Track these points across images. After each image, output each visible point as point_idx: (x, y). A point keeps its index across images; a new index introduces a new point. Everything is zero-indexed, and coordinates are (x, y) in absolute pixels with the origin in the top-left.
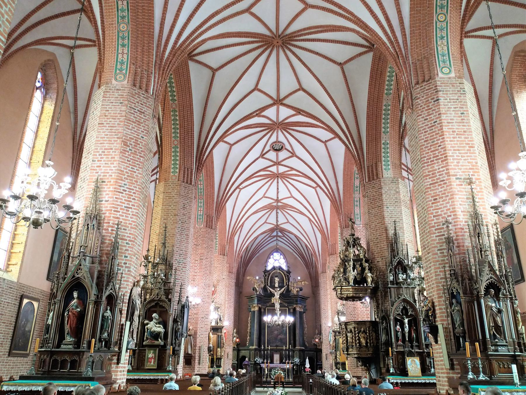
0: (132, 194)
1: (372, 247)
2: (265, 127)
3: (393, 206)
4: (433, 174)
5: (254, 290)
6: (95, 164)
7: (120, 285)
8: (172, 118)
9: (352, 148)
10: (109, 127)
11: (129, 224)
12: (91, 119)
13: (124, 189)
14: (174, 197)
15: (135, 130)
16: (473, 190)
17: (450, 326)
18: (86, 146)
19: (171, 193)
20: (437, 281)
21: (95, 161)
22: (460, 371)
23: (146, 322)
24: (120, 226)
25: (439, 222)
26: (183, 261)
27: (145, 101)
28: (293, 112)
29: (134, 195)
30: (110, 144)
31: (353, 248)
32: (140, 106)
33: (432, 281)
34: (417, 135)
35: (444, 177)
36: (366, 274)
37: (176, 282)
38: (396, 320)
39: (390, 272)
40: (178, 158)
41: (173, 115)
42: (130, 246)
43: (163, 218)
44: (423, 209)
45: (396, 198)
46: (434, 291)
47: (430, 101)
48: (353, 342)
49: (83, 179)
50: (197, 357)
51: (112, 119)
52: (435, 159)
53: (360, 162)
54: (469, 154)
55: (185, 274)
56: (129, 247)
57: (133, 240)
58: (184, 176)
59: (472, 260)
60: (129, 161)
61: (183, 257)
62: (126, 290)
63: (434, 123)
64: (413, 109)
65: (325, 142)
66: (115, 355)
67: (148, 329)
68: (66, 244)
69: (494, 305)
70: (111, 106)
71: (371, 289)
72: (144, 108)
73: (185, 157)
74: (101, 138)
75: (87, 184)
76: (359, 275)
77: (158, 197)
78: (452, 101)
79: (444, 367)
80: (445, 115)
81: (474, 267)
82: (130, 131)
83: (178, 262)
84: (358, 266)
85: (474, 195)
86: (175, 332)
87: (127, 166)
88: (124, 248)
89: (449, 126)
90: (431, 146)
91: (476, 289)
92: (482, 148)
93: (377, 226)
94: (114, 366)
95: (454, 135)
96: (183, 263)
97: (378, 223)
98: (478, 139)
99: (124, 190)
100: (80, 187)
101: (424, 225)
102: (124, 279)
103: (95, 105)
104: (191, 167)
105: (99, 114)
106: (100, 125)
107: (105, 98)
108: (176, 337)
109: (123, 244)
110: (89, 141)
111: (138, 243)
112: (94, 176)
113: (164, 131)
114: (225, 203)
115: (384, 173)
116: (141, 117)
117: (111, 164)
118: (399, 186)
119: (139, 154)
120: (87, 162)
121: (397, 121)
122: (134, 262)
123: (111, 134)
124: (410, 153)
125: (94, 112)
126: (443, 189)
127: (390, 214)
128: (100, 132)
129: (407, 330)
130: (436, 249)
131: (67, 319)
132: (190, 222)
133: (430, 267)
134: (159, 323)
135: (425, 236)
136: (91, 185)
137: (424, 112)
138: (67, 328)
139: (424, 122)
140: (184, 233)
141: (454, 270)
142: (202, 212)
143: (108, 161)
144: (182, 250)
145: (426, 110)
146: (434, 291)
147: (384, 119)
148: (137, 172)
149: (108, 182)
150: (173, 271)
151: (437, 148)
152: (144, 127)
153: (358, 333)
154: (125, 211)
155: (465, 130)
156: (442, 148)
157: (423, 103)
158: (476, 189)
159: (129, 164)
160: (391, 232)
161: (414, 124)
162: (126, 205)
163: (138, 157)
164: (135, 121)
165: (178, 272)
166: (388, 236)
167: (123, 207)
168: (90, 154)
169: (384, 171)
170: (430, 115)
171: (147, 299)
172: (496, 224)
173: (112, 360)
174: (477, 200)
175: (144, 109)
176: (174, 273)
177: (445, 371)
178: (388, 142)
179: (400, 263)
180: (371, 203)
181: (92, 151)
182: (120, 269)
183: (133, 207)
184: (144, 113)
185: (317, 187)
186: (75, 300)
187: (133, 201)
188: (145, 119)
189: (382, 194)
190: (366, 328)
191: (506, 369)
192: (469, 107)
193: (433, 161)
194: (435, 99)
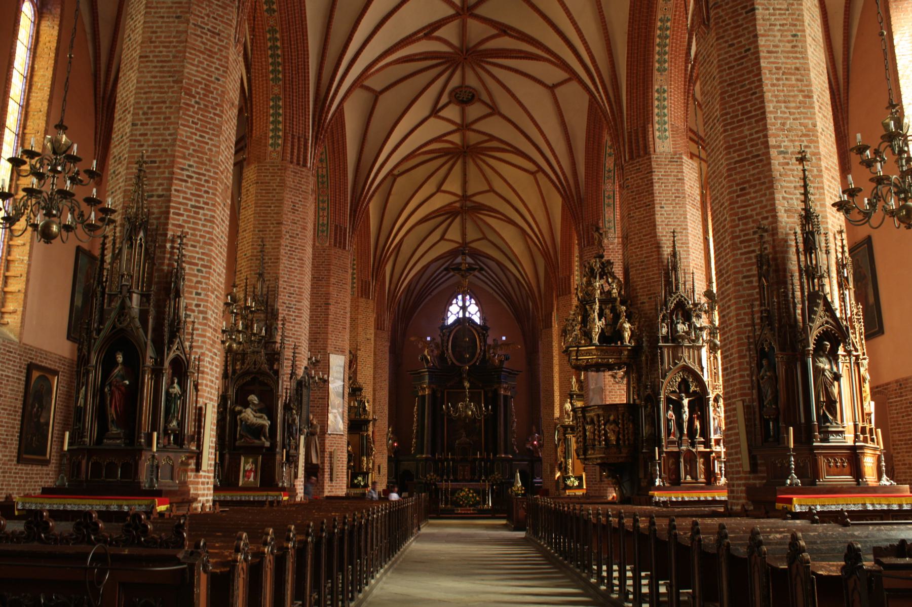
0: (203, 183)
1: (633, 278)
2: (442, 58)
3: (671, 204)
4: (740, 144)
5: (422, 360)
6: (136, 130)
7: (192, 342)
8: (269, 44)
9: (601, 98)
10: (158, 62)
11: (201, 236)
12: (126, 49)
13: (188, 173)
14: (275, 190)
15: (205, 66)
16: (807, 173)
17: (755, 404)
18: (120, 99)
19: (269, 183)
20: (739, 329)
21: (136, 125)
22: (765, 475)
23: (238, 408)
24: (185, 241)
25: (747, 229)
26: (295, 305)
27: (220, 13)
28: (494, 32)
29: (206, 185)
30: (161, 93)
31: (600, 279)
32: (212, 23)
33: (730, 330)
34: (715, 74)
35: (759, 150)
36: (622, 324)
37: (285, 342)
38: (669, 400)
39: (663, 321)
40: (281, 119)
41: (270, 39)
42: (204, 275)
43: (257, 230)
44: (721, 206)
45: (677, 190)
46: (733, 348)
47: (740, 11)
48: (594, 439)
49: (117, 158)
50: (327, 470)
51: (164, 47)
52: (744, 117)
53: (616, 125)
54: (802, 110)
55: (300, 328)
56: (203, 277)
57: (209, 264)
58: (292, 152)
59: (798, 294)
60: (196, 124)
61: (295, 298)
62: (203, 351)
63: (746, 51)
64: (709, 26)
65: (552, 88)
66: (192, 458)
67: (241, 421)
68: (97, 272)
69: (827, 367)
70: (160, 24)
71: (628, 350)
72: (219, 25)
73: (293, 117)
74: (145, 83)
75: (124, 167)
76: (609, 327)
77: (248, 190)
78: (778, 12)
79: (741, 469)
80: (764, 39)
81: (799, 306)
82: (195, 68)
83: (287, 307)
84: (607, 311)
85: (808, 182)
86: (289, 427)
87: (192, 133)
88: (195, 279)
89: (770, 57)
90: (739, 93)
91: (801, 341)
92: (825, 100)
93: (642, 240)
94: (192, 474)
95: (778, 74)
96: (296, 309)
97: (644, 236)
98: (819, 82)
99: (188, 176)
100: (114, 172)
101: (721, 235)
102: (198, 332)
103: (131, 23)
104: (305, 135)
105: (140, 39)
106: (142, 59)
107: (148, 10)
108: (291, 434)
109: (192, 272)
110: (124, 89)
111: (218, 270)
112: (137, 151)
113: (255, 69)
114: (368, 203)
115: (657, 144)
116: (213, 43)
117: (164, 129)
118: (682, 169)
119: (212, 111)
120: (123, 127)
121: (683, 50)
122: (212, 303)
123: (162, 75)
124: (703, 107)
125: (131, 36)
126: (756, 171)
127: (666, 218)
128: (143, 72)
129: (686, 416)
130: (741, 276)
131: (109, 399)
132: (306, 236)
133: (729, 307)
134: (260, 411)
135: (724, 254)
136: (132, 168)
137: (729, 32)
138: (112, 412)
139: (727, 50)
140: (296, 255)
141: (768, 311)
142: (326, 218)
143: (159, 124)
144: (294, 287)
145: (732, 28)
146: (733, 348)
147: (659, 45)
148: (210, 142)
149: (161, 162)
150: (280, 323)
151: (750, 97)
152: (221, 60)
153: (605, 425)
154: (192, 214)
155: (798, 65)
156: (757, 98)
157: (727, 14)
158: (810, 171)
159: (196, 129)
160: (667, 251)
161: (711, 53)
162: (193, 203)
163: (212, 115)
164: (203, 49)
165: (287, 324)
166: (661, 258)
167: (189, 207)
168: (127, 112)
169: (657, 140)
170: (739, 37)
171: (238, 372)
172: (841, 232)
173: (188, 464)
174: (811, 190)
175: (218, 28)
176: (280, 326)
177: (742, 475)
178: (666, 87)
179: (681, 305)
180: (633, 199)
181: (130, 107)
182: (190, 316)
183: (206, 207)
184: (219, 35)
185: (537, 172)
186: (120, 367)
187: (205, 195)
188: (221, 46)
189: (652, 183)
190: (618, 416)
191: (839, 469)
192: (806, 24)
193: (742, 120)
194: (749, 8)
